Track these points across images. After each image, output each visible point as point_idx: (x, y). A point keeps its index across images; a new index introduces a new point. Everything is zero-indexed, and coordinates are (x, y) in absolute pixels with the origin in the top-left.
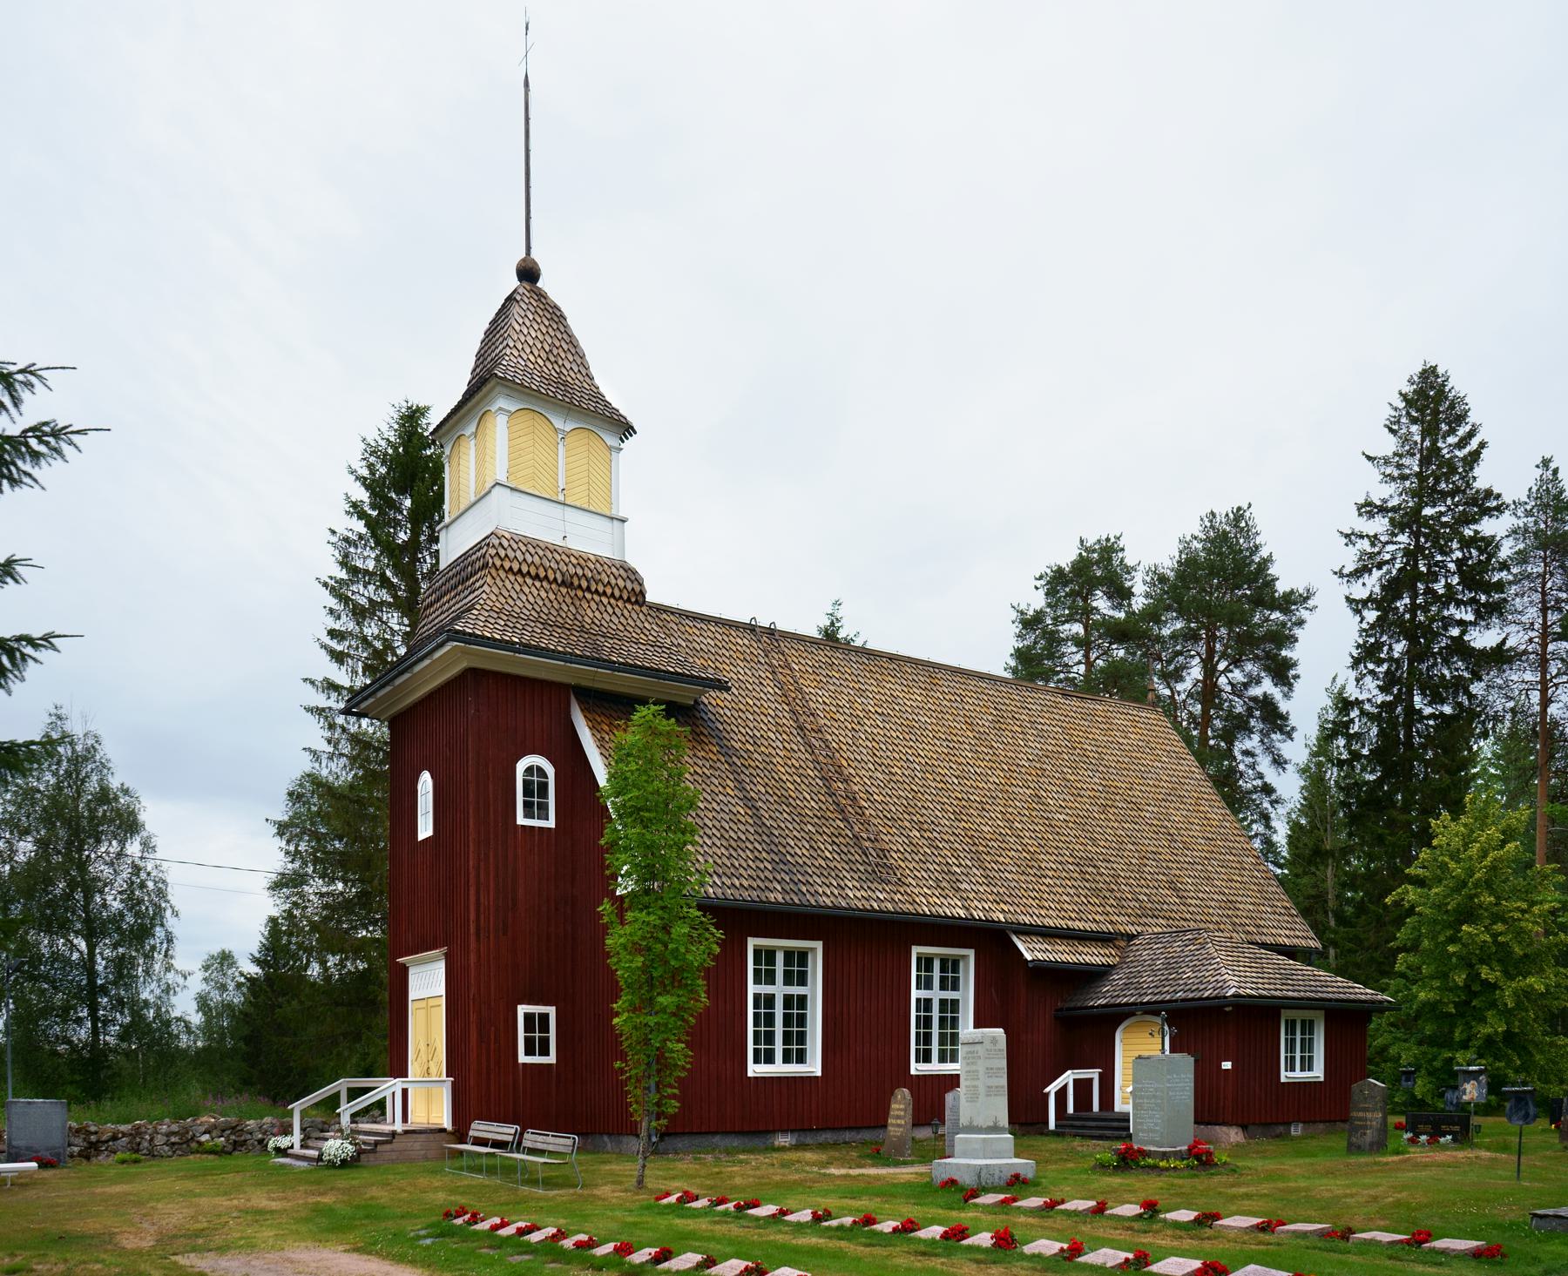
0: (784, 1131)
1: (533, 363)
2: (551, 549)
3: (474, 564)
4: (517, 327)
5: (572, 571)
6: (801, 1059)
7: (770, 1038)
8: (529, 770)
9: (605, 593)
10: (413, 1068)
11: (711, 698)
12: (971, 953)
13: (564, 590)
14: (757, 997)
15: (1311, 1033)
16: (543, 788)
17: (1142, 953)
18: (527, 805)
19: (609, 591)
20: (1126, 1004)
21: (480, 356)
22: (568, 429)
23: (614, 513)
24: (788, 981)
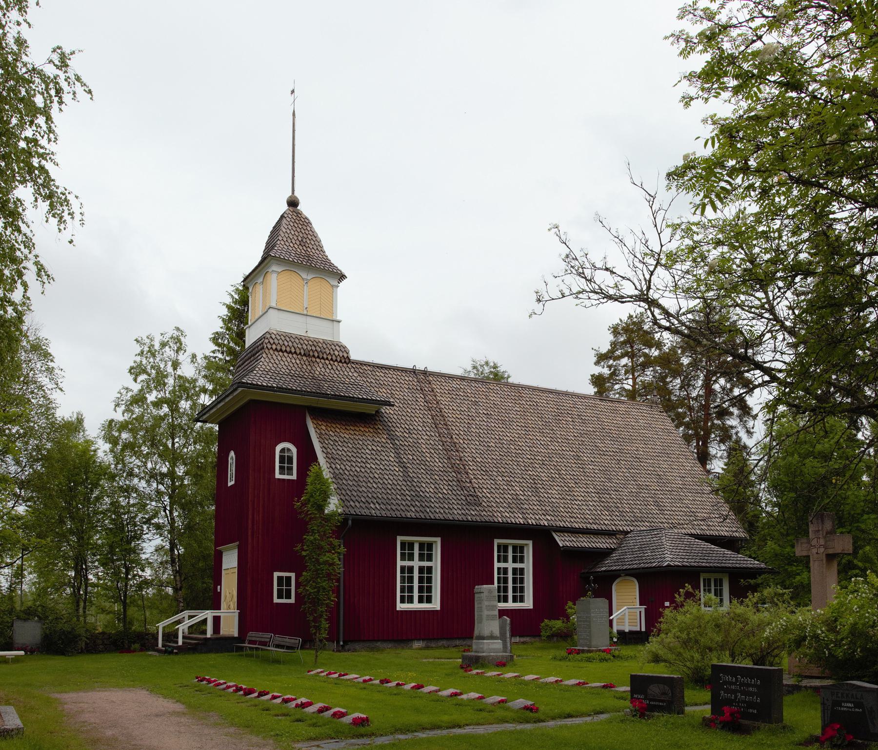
0: (419, 640)
1: (293, 247)
2: (299, 338)
3: (259, 347)
4: (284, 230)
5: (309, 348)
6: (429, 600)
7: (411, 589)
8: (283, 450)
9: (327, 359)
10: (223, 605)
11: (385, 410)
12: (530, 543)
13: (305, 358)
14: (499, 569)
15: (721, 585)
16: (290, 460)
17: (631, 542)
18: (281, 468)
19: (330, 357)
20: (615, 570)
21: (268, 243)
22: (309, 278)
23: (334, 318)
24: (421, 558)
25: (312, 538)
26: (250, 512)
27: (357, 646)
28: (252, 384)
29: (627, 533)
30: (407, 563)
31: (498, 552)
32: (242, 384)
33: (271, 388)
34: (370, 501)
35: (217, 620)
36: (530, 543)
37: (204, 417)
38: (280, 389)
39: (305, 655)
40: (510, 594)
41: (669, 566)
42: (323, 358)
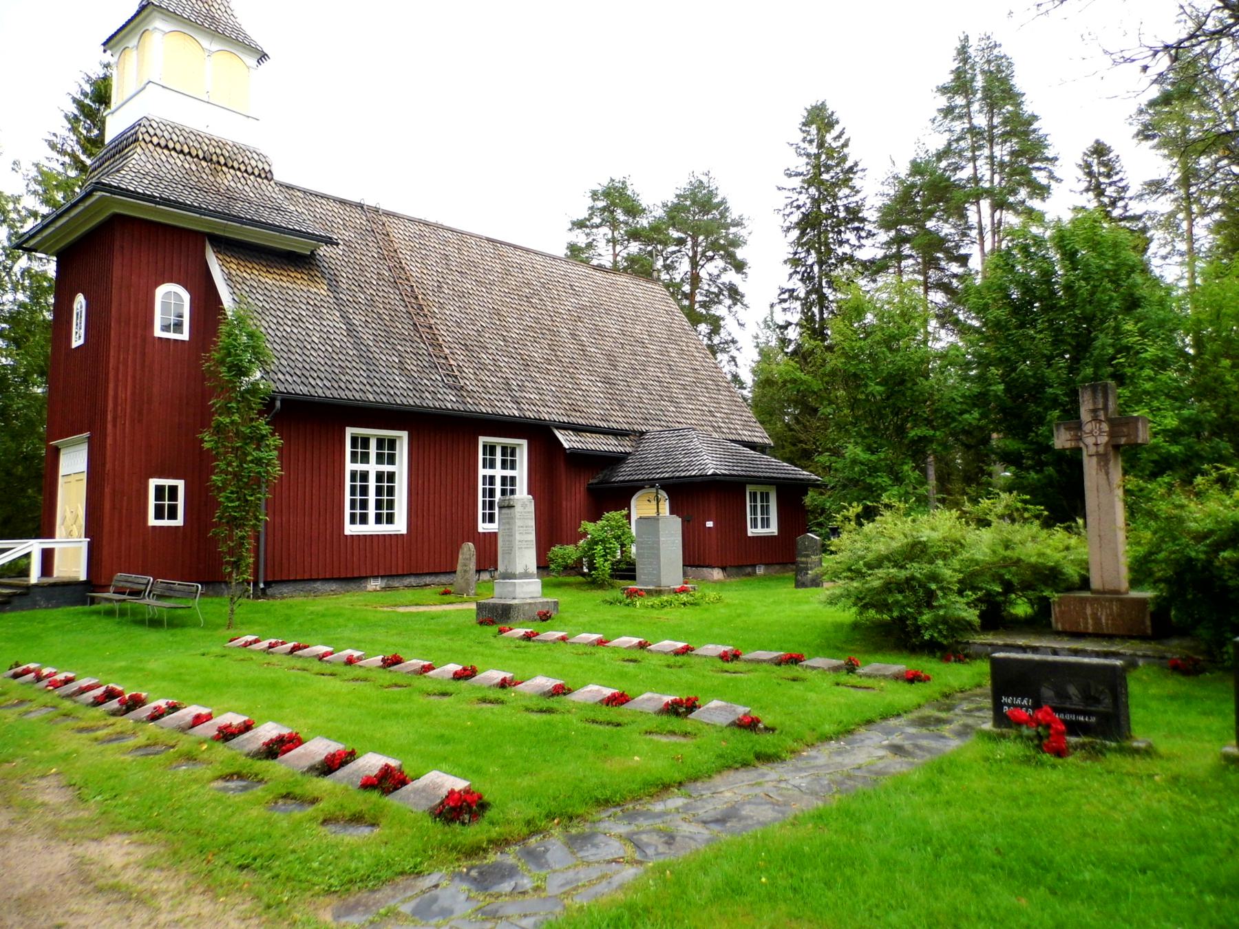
3: (128, 141)
6: (390, 519)
7: (364, 505)
10: (60, 530)
11: (323, 250)
13: (204, 164)
14: (484, 477)
15: (768, 501)
17: (645, 445)
19: (243, 168)
25: (228, 420)
26: (111, 386)
27: (285, 589)
28: (118, 188)
29: (642, 433)
30: (360, 467)
31: (484, 454)
32: (100, 186)
33: (151, 198)
34: (307, 374)
35: (47, 555)
36: (524, 442)
37: (32, 243)
38: (166, 202)
39: (202, 606)
40: (372, 511)
41: (714, 475)
42: (232, 167)
